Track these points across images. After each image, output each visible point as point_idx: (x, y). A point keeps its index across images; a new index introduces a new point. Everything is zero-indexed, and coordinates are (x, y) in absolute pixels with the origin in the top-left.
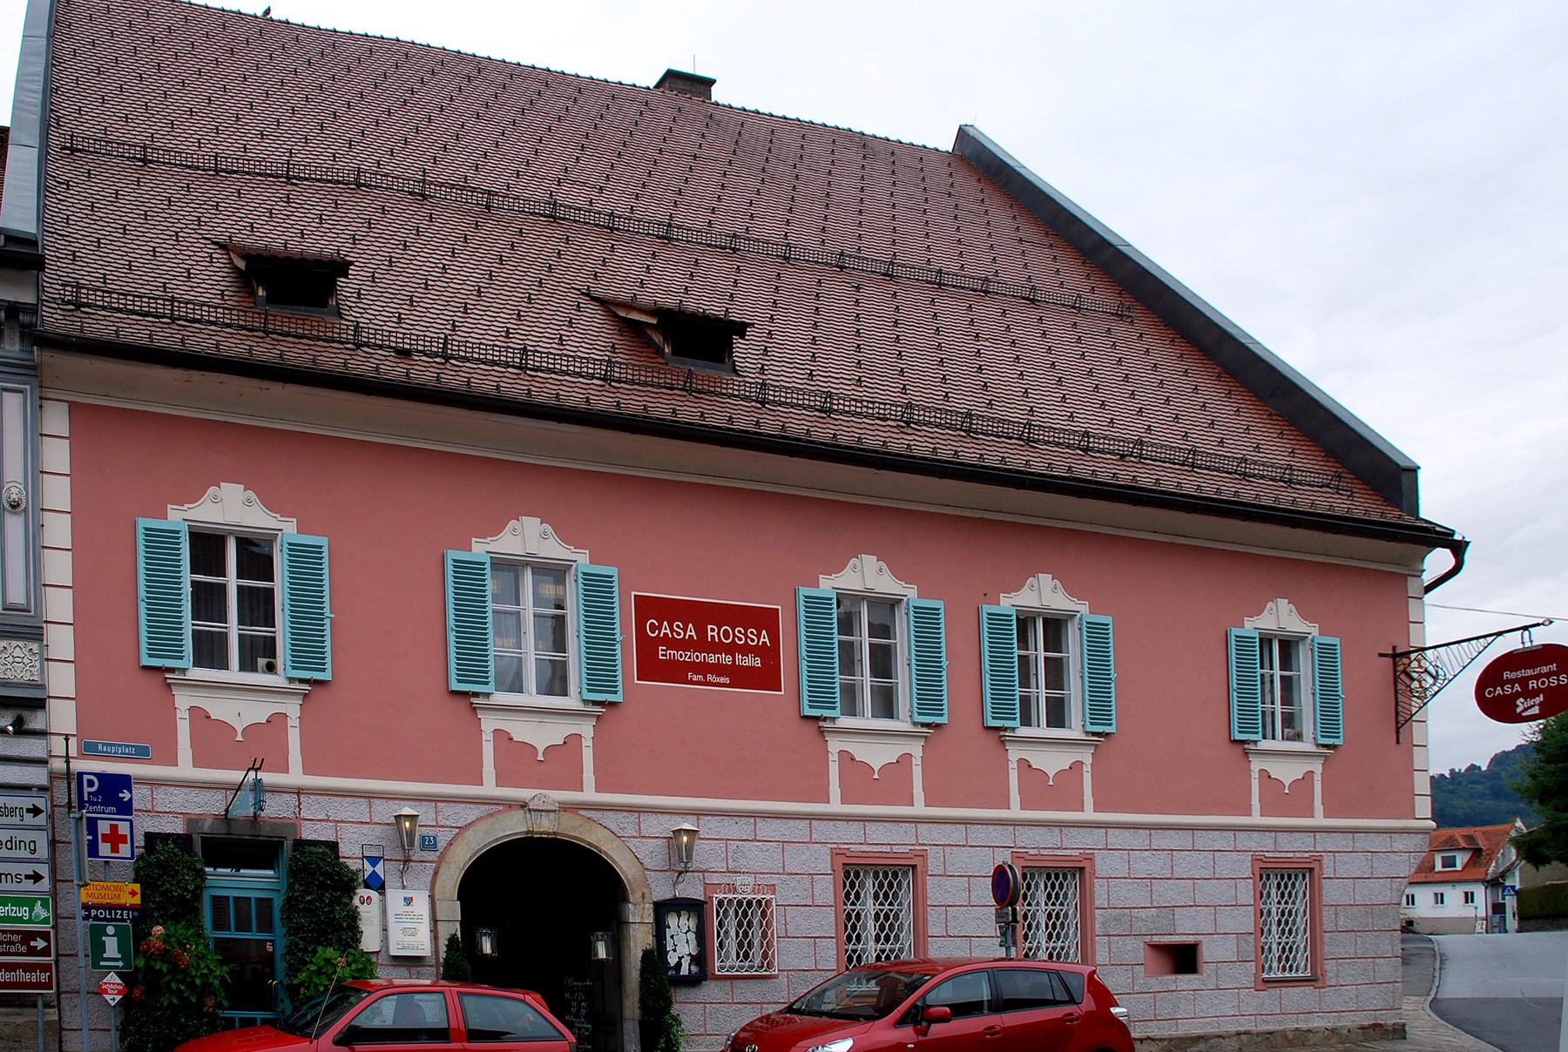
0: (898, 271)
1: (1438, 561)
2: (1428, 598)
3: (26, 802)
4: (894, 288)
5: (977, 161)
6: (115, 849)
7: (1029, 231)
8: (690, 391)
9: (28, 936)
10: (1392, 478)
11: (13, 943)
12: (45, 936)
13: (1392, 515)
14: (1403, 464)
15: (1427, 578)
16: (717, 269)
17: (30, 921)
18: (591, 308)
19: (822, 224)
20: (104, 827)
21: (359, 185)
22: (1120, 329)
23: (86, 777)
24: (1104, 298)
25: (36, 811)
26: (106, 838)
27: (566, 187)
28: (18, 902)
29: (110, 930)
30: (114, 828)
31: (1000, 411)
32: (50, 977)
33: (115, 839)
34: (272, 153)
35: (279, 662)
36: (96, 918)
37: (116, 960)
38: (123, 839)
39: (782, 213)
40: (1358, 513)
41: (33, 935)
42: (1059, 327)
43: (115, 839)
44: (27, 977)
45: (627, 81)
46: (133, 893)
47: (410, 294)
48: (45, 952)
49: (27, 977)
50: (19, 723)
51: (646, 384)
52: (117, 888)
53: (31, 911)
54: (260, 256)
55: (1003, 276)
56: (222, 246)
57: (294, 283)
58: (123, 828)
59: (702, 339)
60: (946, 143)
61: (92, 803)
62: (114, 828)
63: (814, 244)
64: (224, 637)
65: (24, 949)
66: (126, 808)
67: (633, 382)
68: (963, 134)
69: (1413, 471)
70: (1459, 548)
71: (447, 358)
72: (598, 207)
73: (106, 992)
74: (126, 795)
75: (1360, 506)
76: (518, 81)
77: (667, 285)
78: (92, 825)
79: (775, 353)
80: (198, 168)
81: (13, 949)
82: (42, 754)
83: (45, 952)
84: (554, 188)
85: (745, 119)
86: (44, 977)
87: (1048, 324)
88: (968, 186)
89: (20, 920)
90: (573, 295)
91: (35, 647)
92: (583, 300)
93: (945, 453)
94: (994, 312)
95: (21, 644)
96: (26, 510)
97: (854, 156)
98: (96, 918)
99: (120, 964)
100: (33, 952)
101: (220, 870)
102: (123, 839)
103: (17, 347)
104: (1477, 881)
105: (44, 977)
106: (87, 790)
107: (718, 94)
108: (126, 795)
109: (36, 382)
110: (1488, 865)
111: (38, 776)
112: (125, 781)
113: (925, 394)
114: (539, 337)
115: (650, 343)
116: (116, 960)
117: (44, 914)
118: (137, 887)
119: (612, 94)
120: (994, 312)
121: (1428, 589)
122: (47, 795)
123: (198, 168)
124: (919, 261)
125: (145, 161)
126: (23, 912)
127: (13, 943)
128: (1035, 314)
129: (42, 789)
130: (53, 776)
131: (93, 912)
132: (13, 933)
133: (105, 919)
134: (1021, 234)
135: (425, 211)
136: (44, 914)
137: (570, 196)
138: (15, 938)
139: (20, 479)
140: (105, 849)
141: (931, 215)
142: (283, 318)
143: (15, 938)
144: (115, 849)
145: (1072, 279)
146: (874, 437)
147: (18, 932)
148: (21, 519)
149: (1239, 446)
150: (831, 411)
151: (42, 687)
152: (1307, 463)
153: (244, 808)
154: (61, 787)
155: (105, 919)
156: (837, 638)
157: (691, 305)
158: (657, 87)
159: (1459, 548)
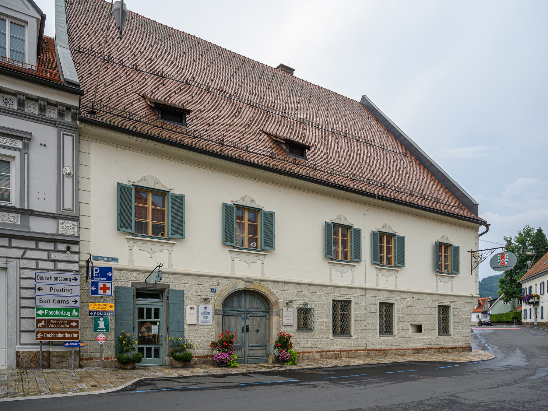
0: (348, 135)
1: (482, 229)
2: (479, 238)
3: (72, 276)
4: (347, 140)
5: (366, 106)
6: (105, 292)
7: (381, 128)
8: (295, 164)
9: (69, 322)
10: (473, 207)
11: (64, 324)
12: (77, 321)
13: (473, 216)
14: (475, 203)
15: (480, 233)
16: (298, 128)
17: (71, 316)
18: (264, 135)
19: (327, 119)
20: (101, 285)
21: (187, 84)
22: (405, 159)
23: (94, 268)
24: (401, 150)
25: (76, 279)
26: (101, 288)
27: (253, 96)
28: (66, 310)
29: (102, 319)
30: (105, 285)
31: (376, 178)
32: (78, 336)
33: (105, 289)
34: (156, 68)
35: (166, 233)
36: (96, 315)
37: (103, 329)
38: (108, 289)
39: (315, 114)
40: (464, 215)
41: (72, 321)
42: (390, 156)
43: (105, 289)
44: (69, 336)
45: (242, 54)
46: (111, 307)
47: (207, 121)
48: (77, 327)
49: (69, 336)
50: (68, 248)
51: (282, 160)
52: (104, 305)
53: (71, 313)
54: (160, 104)
55: (375, 141)
56: (143, 97)
57: (175, 114)
58: (108, 285)
59: (298, 149)
60: (359, 100)
61: (96, 277)
62: (105, 285)
63: (325, 124)
64: (147, 224)
65: (68, 326)
66: (110, 278)
67: (279, 159)
68: (364, 98)
69: (477, 205)
70: (487, 226)
71: (223, 145)
72: (263, 103)
73: (99, 340)
74: (110, 274)
75: (464, 212)
76: (235, 58)
77: (285, 131)
78: (95, 284)
79: (317, 155)
80: (129, 67)
81: (64, 326)
82: (77, 260)
83: (77, 327)
84: (209, 81)
85: (303, 84)
86: (75, 335)
87: (387, 156)
88: (365, 113)
89: (67, 316)
90: (258, 130)
91: (75, 223)
92: (261, 132)
93: (363, 189)
94: (373, 150)
95: (69, 222)
96: (73, 177)
97: (334, 99)
98: (96, 315)
99: (105, 330)
100: (72, 327)
101: (147, 299)
102: (108, 289)
103: (70, 121)
104: (479, 312)
105: (75, 335)
106: (95, 272)
107: (295, 74)
108: (110, 274)
109: (77, 133)
110: (482, 308)
111: (76, 267)
112: (110, 269)
113: (357, 173)
114: (250, 141)
115: (282, 148)
116: (103, 329)
117: (76, 314)
118: (113, 305)
119: (263, 69)
120: (373, 150)
121: (480, 236)
122: (78, 273)
123: (129, 67)
124: (353, 133)
125: (108, 60)
126: (68, 313)
127: (64, 324)
128: (384, 152)
129: (77, 271)
130: (80, 267)
131: (95, 313)
132: (63, 320)
133: (100, 315)
134: (379, 129)
135: (209, 96)
136: (76, 314)
137: (255, 99)
138: (64, 322)
139: (70, 165)
140: (101, 292)
141: (356, 120)
142: (169, 124)
143: (64, 322)
144: (105, 292)
145: (392, 144)
146: (346, 183)
147: (66, 320)
148: (70, 179)
149: (435, 195)
150: (333, 174)
151: (79, 237)
152: (452, 201)
153: (152, 280)
154: (84, 271)
155: (100, 315)
156: (333, 236)
157: (293, 138)
158: (278, 68)
159: (487, 226)
